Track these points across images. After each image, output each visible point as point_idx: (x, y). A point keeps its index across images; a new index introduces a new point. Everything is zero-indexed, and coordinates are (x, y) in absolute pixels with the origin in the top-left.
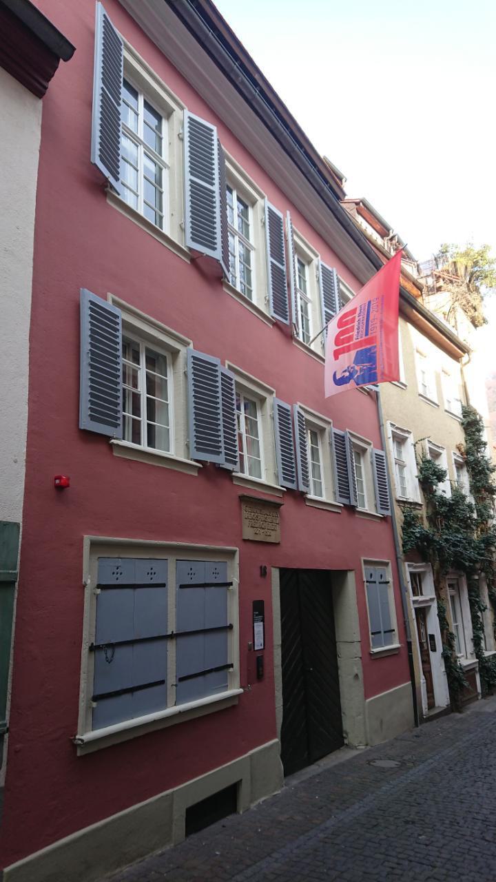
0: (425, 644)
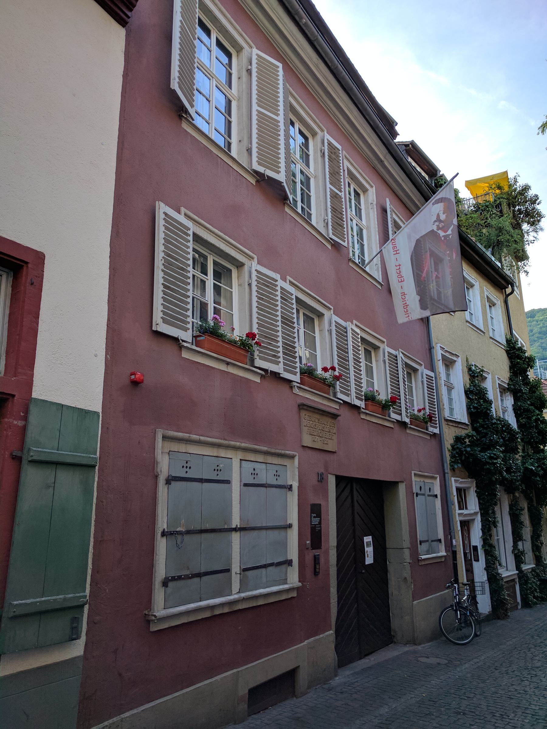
0: (468, 555)
